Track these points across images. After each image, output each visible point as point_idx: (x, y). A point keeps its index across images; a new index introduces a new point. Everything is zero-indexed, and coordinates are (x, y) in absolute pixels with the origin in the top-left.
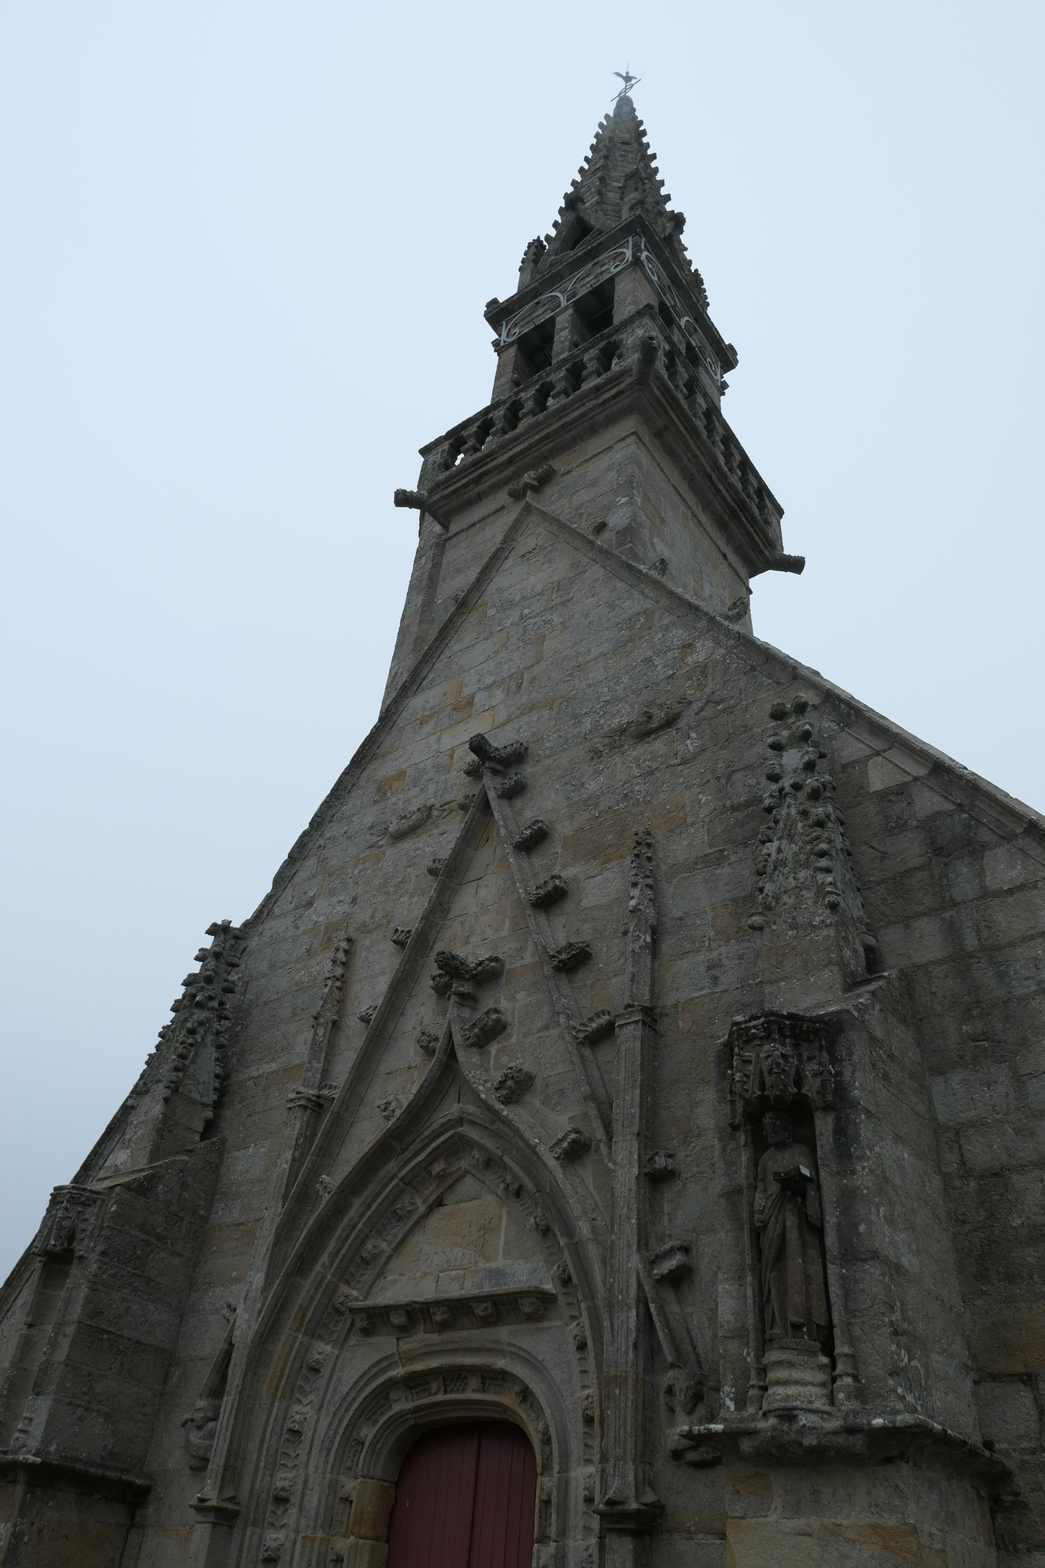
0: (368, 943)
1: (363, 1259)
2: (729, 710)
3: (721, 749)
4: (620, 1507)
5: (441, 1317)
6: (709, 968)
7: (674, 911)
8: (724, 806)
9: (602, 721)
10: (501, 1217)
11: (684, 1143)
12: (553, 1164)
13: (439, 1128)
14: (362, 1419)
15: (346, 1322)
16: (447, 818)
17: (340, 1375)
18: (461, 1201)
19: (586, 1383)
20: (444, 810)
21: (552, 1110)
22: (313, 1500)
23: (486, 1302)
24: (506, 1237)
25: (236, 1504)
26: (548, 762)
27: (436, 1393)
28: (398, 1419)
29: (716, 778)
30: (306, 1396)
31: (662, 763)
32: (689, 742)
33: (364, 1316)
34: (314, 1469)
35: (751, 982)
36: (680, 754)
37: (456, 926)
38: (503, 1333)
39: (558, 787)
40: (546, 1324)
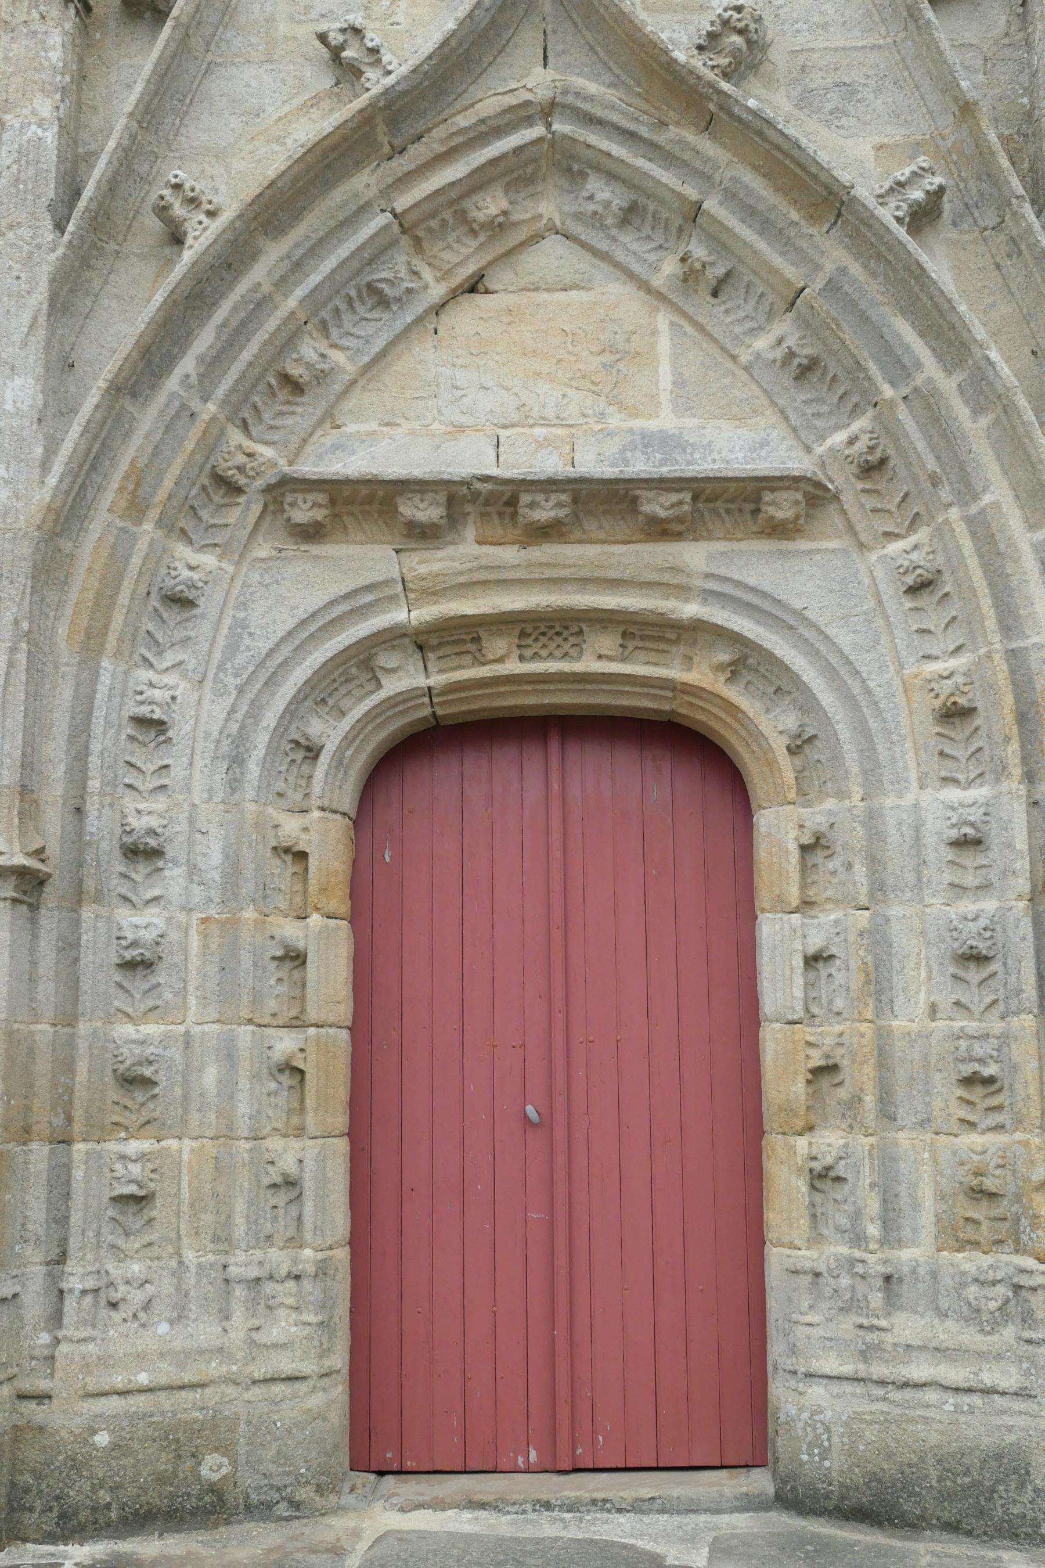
1: (286, 379)
5: (552, 514)
10: (654, 332)
12: (901, 232)
13: (498, 115)
14: (309, 703)
15: (248, 508)
17: (242, 615)
18: (537, 289)
19: (930, 652)
23: (679, 491)
24: (677, 373)
25: (43, 861)
27: (500, 660)
28: (396, 705)
30: (160, 654)
33: (321, 498)
34: (205, 795)
40: (802, 545)
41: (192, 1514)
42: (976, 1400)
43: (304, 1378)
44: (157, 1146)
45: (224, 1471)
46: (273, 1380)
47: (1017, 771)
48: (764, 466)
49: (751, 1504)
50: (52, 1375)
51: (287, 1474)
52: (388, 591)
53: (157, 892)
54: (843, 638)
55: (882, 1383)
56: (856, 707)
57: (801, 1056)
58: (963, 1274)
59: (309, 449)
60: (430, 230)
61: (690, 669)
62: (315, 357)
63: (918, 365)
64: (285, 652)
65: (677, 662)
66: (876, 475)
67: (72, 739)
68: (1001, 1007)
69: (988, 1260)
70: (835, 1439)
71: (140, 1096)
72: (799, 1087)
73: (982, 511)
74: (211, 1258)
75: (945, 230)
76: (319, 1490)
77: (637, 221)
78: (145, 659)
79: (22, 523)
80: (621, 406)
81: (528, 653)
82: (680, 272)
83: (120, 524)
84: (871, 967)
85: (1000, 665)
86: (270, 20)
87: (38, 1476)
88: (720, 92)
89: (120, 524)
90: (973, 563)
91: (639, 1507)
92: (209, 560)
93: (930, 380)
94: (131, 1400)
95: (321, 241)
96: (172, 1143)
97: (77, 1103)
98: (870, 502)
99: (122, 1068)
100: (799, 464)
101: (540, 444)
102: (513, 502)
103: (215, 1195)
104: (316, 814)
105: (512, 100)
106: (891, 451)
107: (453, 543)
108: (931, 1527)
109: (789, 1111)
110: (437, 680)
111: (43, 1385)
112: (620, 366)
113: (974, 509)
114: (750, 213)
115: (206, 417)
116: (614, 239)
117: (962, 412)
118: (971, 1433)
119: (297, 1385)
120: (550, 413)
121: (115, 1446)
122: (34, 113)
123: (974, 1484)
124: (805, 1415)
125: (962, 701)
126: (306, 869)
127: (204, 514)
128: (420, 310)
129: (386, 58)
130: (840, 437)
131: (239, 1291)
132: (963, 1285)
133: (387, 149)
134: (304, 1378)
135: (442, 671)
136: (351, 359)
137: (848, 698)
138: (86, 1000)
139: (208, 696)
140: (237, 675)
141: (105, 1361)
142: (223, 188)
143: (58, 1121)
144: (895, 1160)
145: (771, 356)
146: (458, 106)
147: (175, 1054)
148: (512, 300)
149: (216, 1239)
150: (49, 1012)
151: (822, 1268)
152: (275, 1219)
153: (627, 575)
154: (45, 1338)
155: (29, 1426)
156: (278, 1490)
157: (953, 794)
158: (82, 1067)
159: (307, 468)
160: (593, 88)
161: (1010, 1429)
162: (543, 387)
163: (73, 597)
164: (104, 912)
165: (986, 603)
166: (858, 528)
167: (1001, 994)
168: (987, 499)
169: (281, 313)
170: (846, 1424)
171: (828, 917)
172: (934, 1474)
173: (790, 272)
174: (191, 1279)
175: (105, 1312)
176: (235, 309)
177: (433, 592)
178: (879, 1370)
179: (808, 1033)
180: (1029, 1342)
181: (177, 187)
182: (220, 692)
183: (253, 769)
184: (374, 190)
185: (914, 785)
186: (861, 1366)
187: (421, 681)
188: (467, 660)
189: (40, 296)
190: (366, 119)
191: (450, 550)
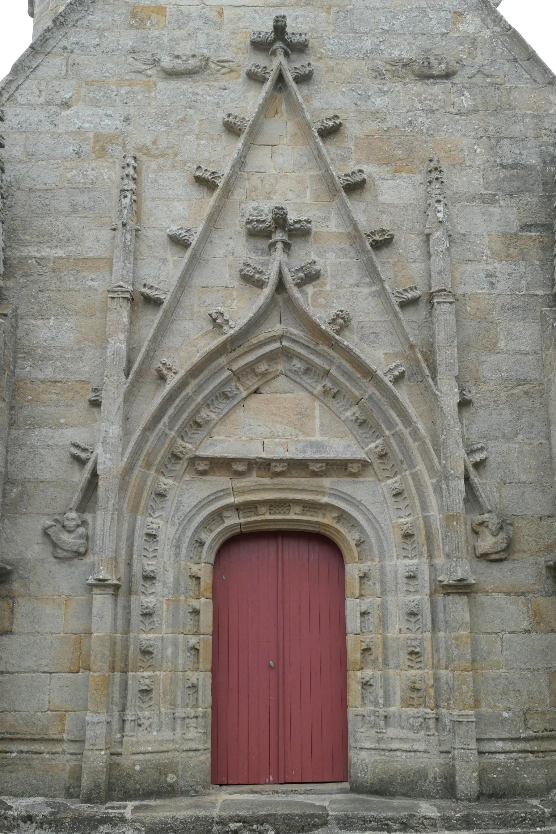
0: (154, 166)
2: (497, 86)
3: (490, 115)
4: (465, 582)
6: (488, 276)
7: (459, 227)
8: (495, 162)
9: (382, 47)
10: (314, 408)
11: (475, 385)
12: (390, 385)
14: (201, 528)
16: (228, 75)
17: (180, 499)
20: (224, 67)
21: (370, 346)
22: (170, 579)
26: (331, 63)
27: (263, 514)
29: (488, 137)
30: (154, 512)
31: (441, 107)
32: (463, 98)
33: (207, 463)
35: (518, 293)
36: (456, 105)
37: (255, 180)
38: (327, 482)
39: (344, 90)
40: (361, 479)
41: (165, 793)
42: (412, 754)
43: (199, 750)
44: (153, 674)
45: (174, 779)
46: (189, 750)
47: (426, 555)
48: (348, 456)
49: (343, 791)
50: (122, 747)
51: (194, 781)
52: (228, 492)
53: (153, 591)
54: (373, 510)
55: (384, 750)
56: (378, 532)
57: (359, 645)
58: (409, 715)
59: (202, 444)
60: (243, 375)
61: (324, 518)
62: (205, 416)
63: (397, 425)
64: (194, 511)
65: (320, 516)
66: (384, 458)
67: (128, 540)
68: (421, 629)
69: (417, 710)
70: (369, 769)
71: (147, 657)
72: (358, 656)
73: (416, 472)
74: (169, 711)
75: (405, 383)
76: (203, 787)
77: (309, 372)
78: (150, 514)
79: (115, 473)
80: (303, 432)
81: (272, 512)
82: (323, 390)
83: (143, 470)
84: (381, 617)
85: (421, 522)
86: (192, 305)
87: (117, 780)
88: (336, 339)
89: (143, 470)
90: (413, 488)
91: (306, 792)
92: (170, 481)
93: (400, 430)
94: (146, 756)
95: (208, 379)
96: (158, 673)
97: (130, 660)
98: (382, 467)
99: (143, 648)
100: (361, 455)
101: (278, 444)
102: (269, 465)
103: (170, 690)
104: (203, 565)
105: (270, 335)
106: (388, 451)
107: (249, 477)
108: (398, 795)
109: (355, 663)
110: (243, 520)
111: (119, 750)
112: (303, 419)
113: (414, 471)
114: (345, 373)
115: (171, 436)
116: (302, 378)
117: (410, 440)
118: (410, 765)
119: (197, 752)
120: (280, 434)
121: (141, 770)
122: (118, 339)
123: (412, 780)
124: (360, 761)
125: (410, 532)
126: (199, 583)
127: (169, 466)
128: (239, 400)
129: (231, 323)
130: (373, 445)
131: (179, 721)
132: (409, 718)
133: (230, 350)
134: (199, 750)
135: (244, 517)
136: (216, 416)
137: (375, 529)
138: (133, 626)
139: (169, 526)
140: (178, 519)
141: (138, 743)
142: (177, 361)
143: (122, 665)
144: (388, 679)
145: (351, 418)
146: (253, 336)
147: (159, 643)
148: (269, 396)
149: (171, 705)
150: (120, 630)
151: (365, 714)
152: (189, 698)
153: (305, 487)
154: (119, 736)
155: (114, 763)
156: (191, 786)
157: (407, 561)
158: (131, 648)
159: (202, 453)
160: (296, 332)
161: (422, 763)
162: (278, 425)
163: (128, 495)
164: (138, 597)
165: (417, 502)
166: (378, 475)
167: (421, 626)
168: (418, 468)
169: (196, 403)
170: (372, 764)
171: (369, 600)
172: (399, 778)
173: (357, 394)
174: (163, 717)
175: (137, 727)
176: (180, 401)
177: (242, 492)
178: (382, 746)
179: (362, 638)
180: (428, 735)
181: (164, 364)
182: (173, 525)
183: (184, 550)
184: (226, 363)
185: (395, 558)
186: (377, 745)
187: (237, 521)
188: (252, 514)
189: (121, 399)
190: (224, 343)
191: (248, 479)
